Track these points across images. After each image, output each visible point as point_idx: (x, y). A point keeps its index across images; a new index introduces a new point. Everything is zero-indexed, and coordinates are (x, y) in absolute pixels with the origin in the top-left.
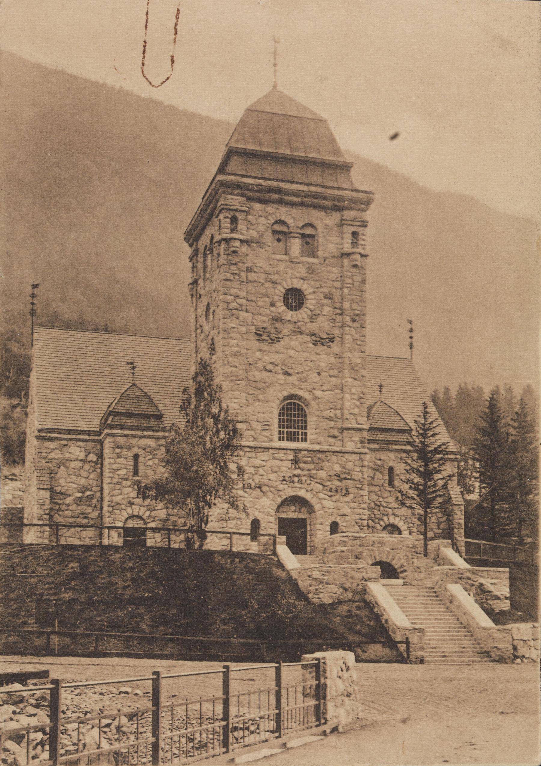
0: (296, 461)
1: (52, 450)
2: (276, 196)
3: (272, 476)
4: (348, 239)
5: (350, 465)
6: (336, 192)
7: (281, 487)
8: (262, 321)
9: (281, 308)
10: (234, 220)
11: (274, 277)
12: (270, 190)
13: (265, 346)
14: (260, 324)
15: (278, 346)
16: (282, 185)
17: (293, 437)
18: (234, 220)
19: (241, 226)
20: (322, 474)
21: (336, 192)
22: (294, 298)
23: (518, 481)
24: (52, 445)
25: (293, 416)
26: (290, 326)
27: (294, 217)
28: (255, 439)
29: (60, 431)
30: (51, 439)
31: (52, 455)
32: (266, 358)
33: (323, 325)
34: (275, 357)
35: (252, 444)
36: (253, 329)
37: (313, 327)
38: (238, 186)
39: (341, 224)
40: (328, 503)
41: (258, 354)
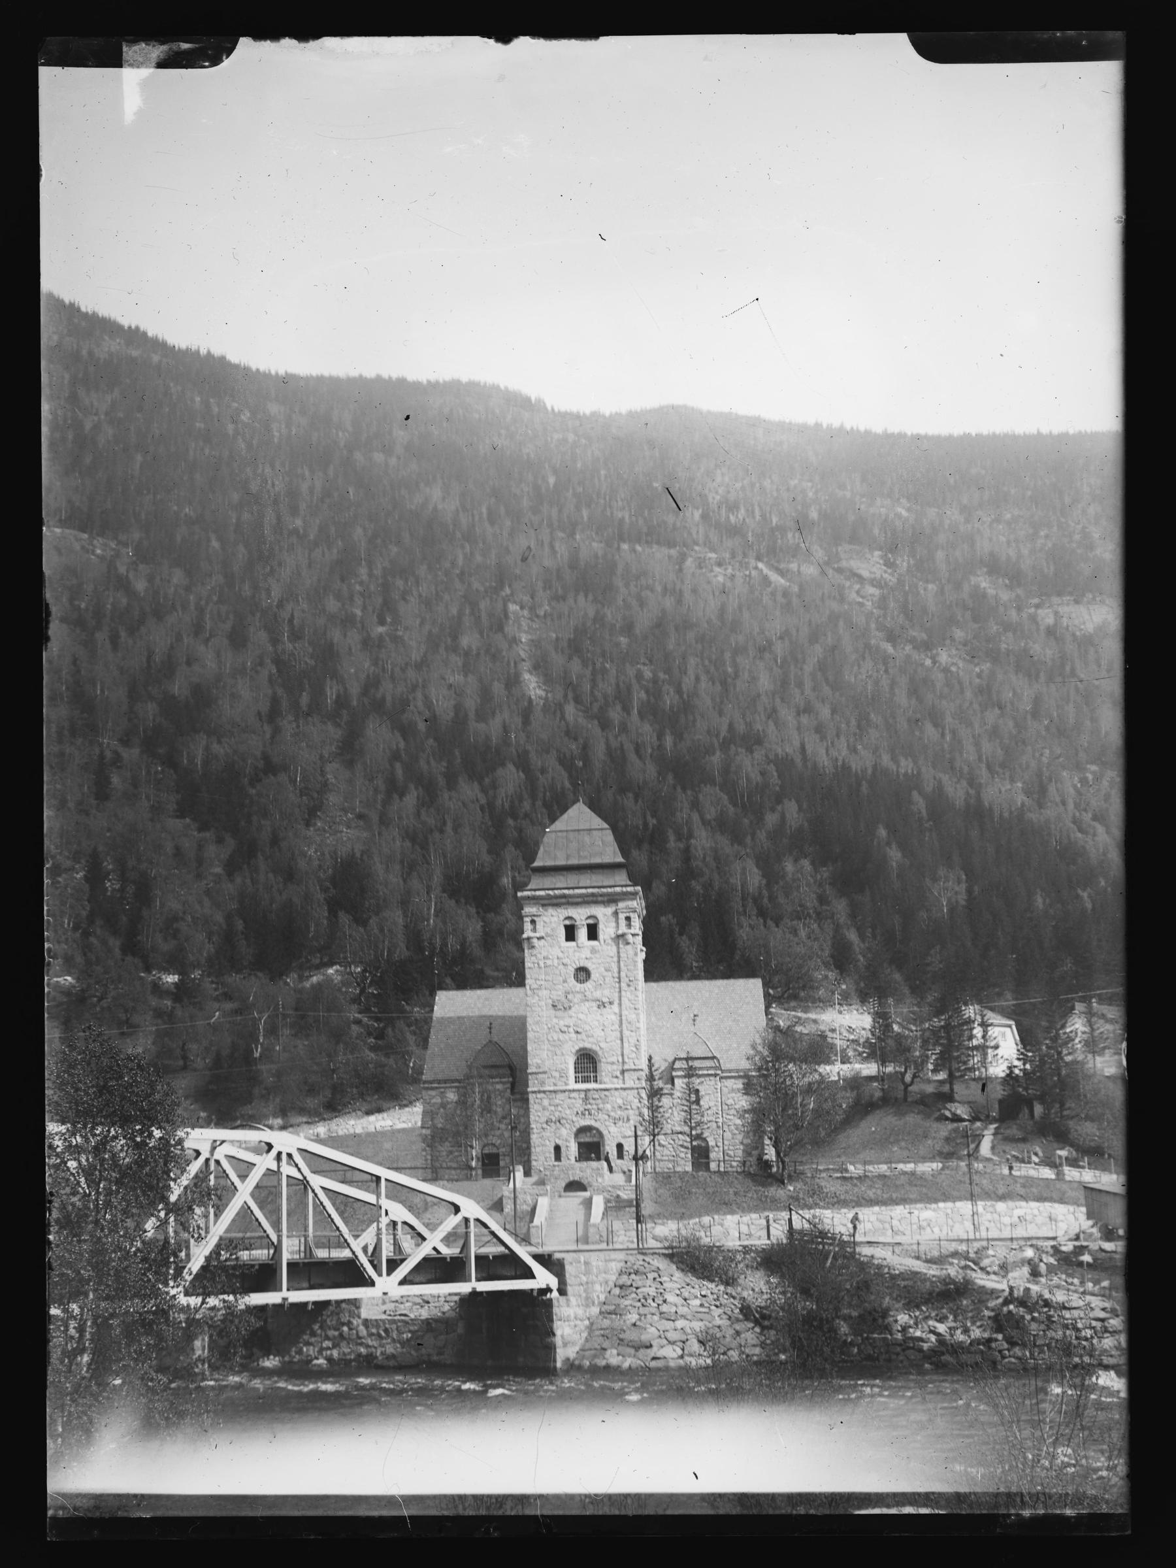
0: (586, 1099)
1: (434, 1097)
2: (563, 900)
3: (568, 1112)
4: (623, 922)
5: (630, 1098)
6: (609, 890)
7: (575, 1119)
8: (558, 994)
9: (572, 981)
10: (533, 922)
11: (565, 961)
12: (556, 897)
13: (559, 1013)
14: (555, 998)
15: (571, 1012)
16: (566, 892)
17: (586, 1080)
18: (533, 922)
19: (539, 926)
20: (609, 1106)
21: (609, 890)
22: (583, 973)
23: (59, 1150)
24: (433, 1093)
25: (587, 1063)
26: (579, 996)
27: (580, 915)
28: (555, 1085)
29: (439, 1082)
30: (432, 1089)
31: (434, 1101)
32: (562, 1023)
33: (606, 994)
34: (568, 1021)
35: (552, 1088)
36: (550, 1002)
37: (598, 994)
38: (534, 898)
39: (616, 913)
40: (613, 1129)
41: (555, 1020)
